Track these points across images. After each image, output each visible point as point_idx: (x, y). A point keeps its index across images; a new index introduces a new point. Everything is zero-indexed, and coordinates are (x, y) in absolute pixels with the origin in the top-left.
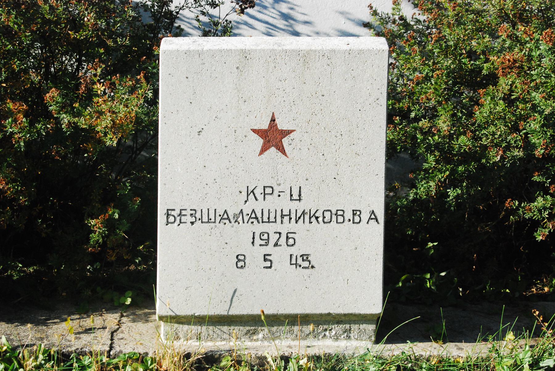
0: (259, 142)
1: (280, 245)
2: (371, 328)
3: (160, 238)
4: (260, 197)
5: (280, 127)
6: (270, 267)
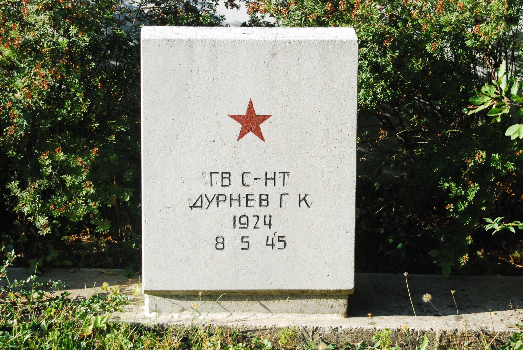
0: (238, 127)
1: (258, 228)
2: (343, 302)
3: (145, 257)
5: (256, 114)
6: (243, 238)
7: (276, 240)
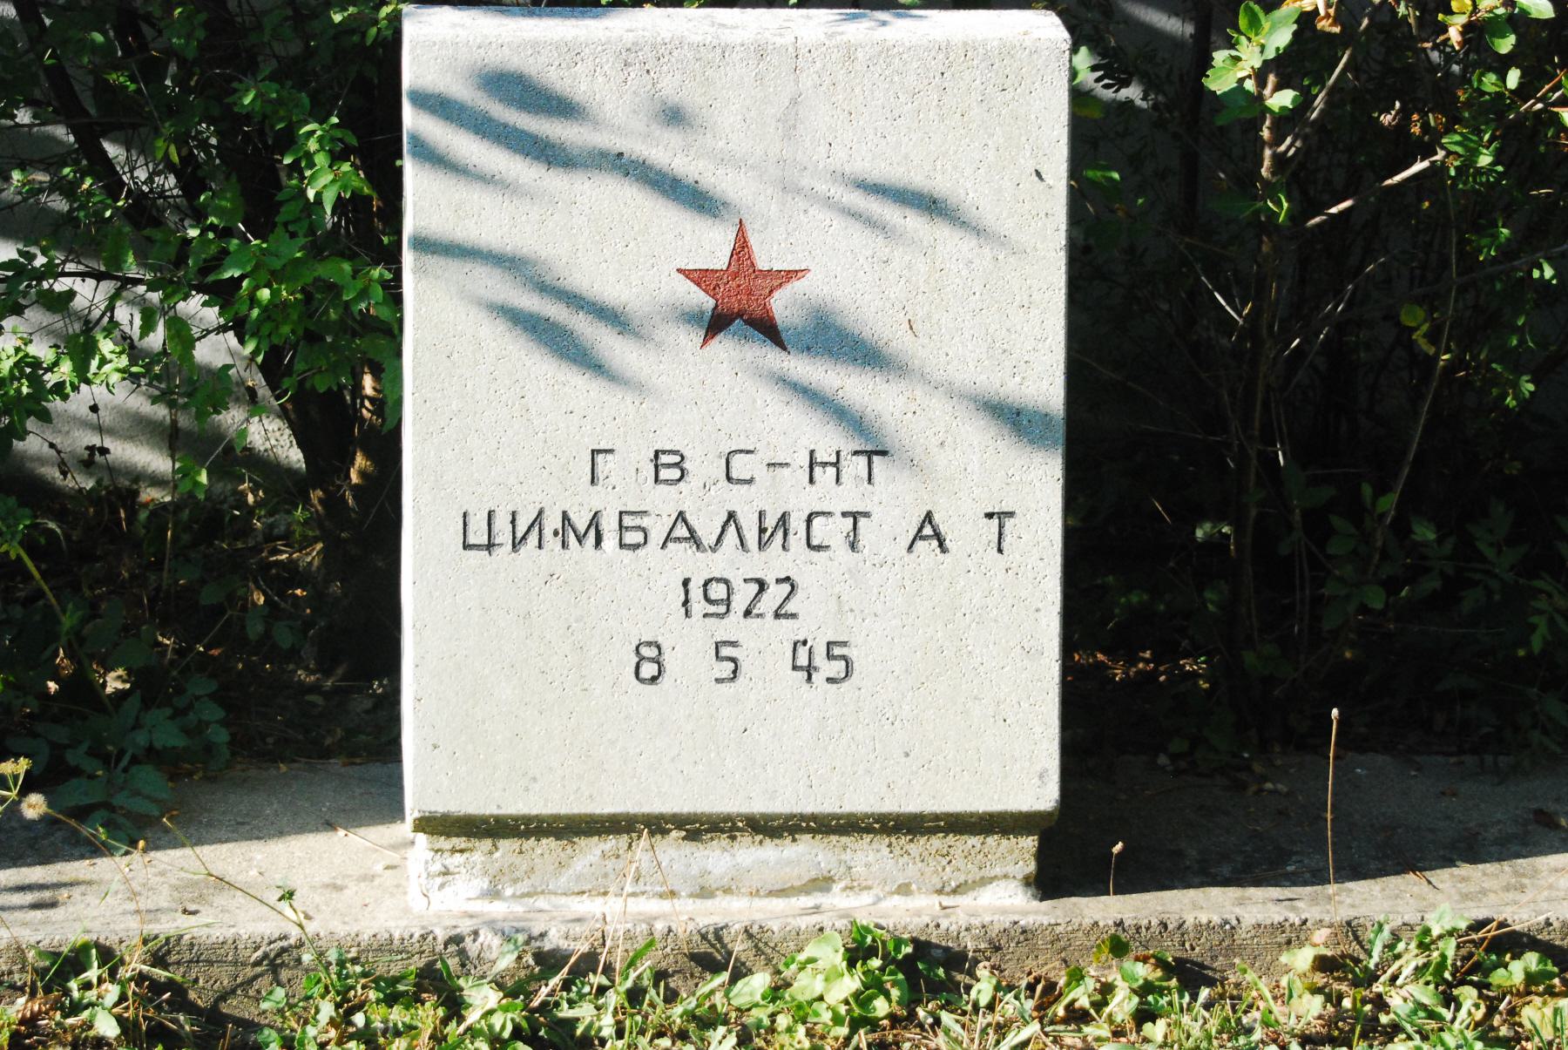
2: (1030, 843)
7: (820, 651)
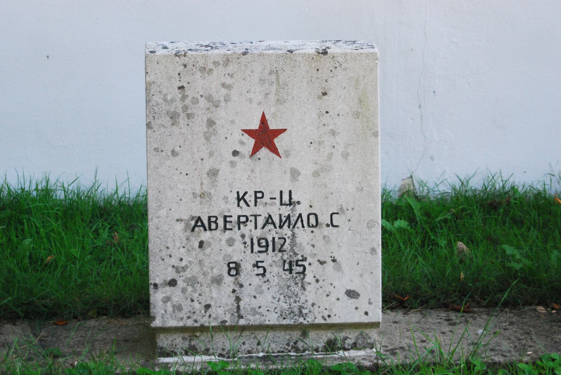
4: (252, 204)
